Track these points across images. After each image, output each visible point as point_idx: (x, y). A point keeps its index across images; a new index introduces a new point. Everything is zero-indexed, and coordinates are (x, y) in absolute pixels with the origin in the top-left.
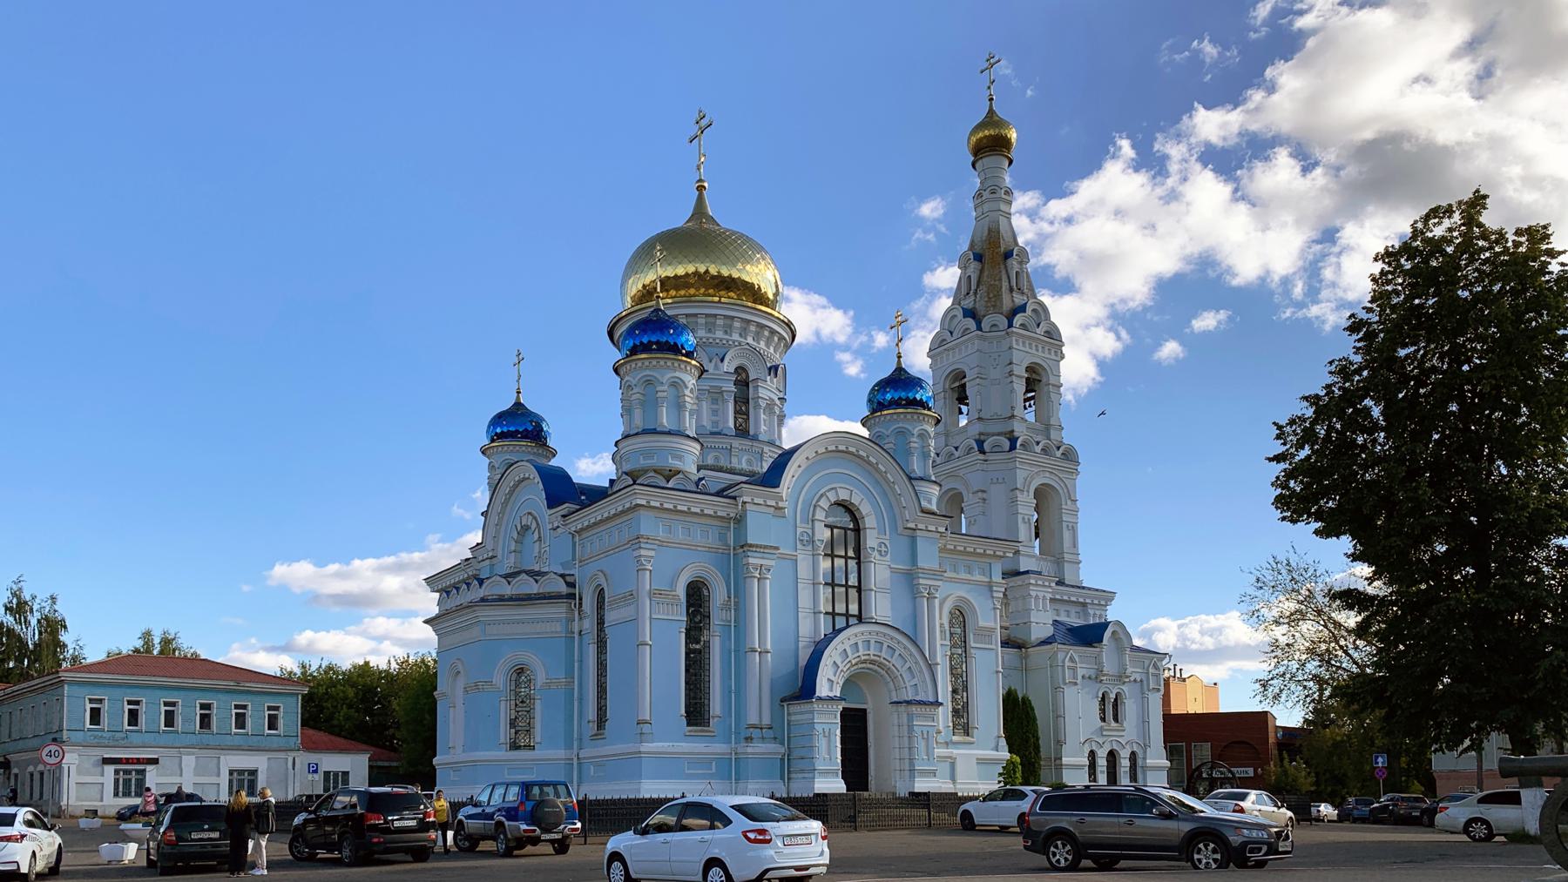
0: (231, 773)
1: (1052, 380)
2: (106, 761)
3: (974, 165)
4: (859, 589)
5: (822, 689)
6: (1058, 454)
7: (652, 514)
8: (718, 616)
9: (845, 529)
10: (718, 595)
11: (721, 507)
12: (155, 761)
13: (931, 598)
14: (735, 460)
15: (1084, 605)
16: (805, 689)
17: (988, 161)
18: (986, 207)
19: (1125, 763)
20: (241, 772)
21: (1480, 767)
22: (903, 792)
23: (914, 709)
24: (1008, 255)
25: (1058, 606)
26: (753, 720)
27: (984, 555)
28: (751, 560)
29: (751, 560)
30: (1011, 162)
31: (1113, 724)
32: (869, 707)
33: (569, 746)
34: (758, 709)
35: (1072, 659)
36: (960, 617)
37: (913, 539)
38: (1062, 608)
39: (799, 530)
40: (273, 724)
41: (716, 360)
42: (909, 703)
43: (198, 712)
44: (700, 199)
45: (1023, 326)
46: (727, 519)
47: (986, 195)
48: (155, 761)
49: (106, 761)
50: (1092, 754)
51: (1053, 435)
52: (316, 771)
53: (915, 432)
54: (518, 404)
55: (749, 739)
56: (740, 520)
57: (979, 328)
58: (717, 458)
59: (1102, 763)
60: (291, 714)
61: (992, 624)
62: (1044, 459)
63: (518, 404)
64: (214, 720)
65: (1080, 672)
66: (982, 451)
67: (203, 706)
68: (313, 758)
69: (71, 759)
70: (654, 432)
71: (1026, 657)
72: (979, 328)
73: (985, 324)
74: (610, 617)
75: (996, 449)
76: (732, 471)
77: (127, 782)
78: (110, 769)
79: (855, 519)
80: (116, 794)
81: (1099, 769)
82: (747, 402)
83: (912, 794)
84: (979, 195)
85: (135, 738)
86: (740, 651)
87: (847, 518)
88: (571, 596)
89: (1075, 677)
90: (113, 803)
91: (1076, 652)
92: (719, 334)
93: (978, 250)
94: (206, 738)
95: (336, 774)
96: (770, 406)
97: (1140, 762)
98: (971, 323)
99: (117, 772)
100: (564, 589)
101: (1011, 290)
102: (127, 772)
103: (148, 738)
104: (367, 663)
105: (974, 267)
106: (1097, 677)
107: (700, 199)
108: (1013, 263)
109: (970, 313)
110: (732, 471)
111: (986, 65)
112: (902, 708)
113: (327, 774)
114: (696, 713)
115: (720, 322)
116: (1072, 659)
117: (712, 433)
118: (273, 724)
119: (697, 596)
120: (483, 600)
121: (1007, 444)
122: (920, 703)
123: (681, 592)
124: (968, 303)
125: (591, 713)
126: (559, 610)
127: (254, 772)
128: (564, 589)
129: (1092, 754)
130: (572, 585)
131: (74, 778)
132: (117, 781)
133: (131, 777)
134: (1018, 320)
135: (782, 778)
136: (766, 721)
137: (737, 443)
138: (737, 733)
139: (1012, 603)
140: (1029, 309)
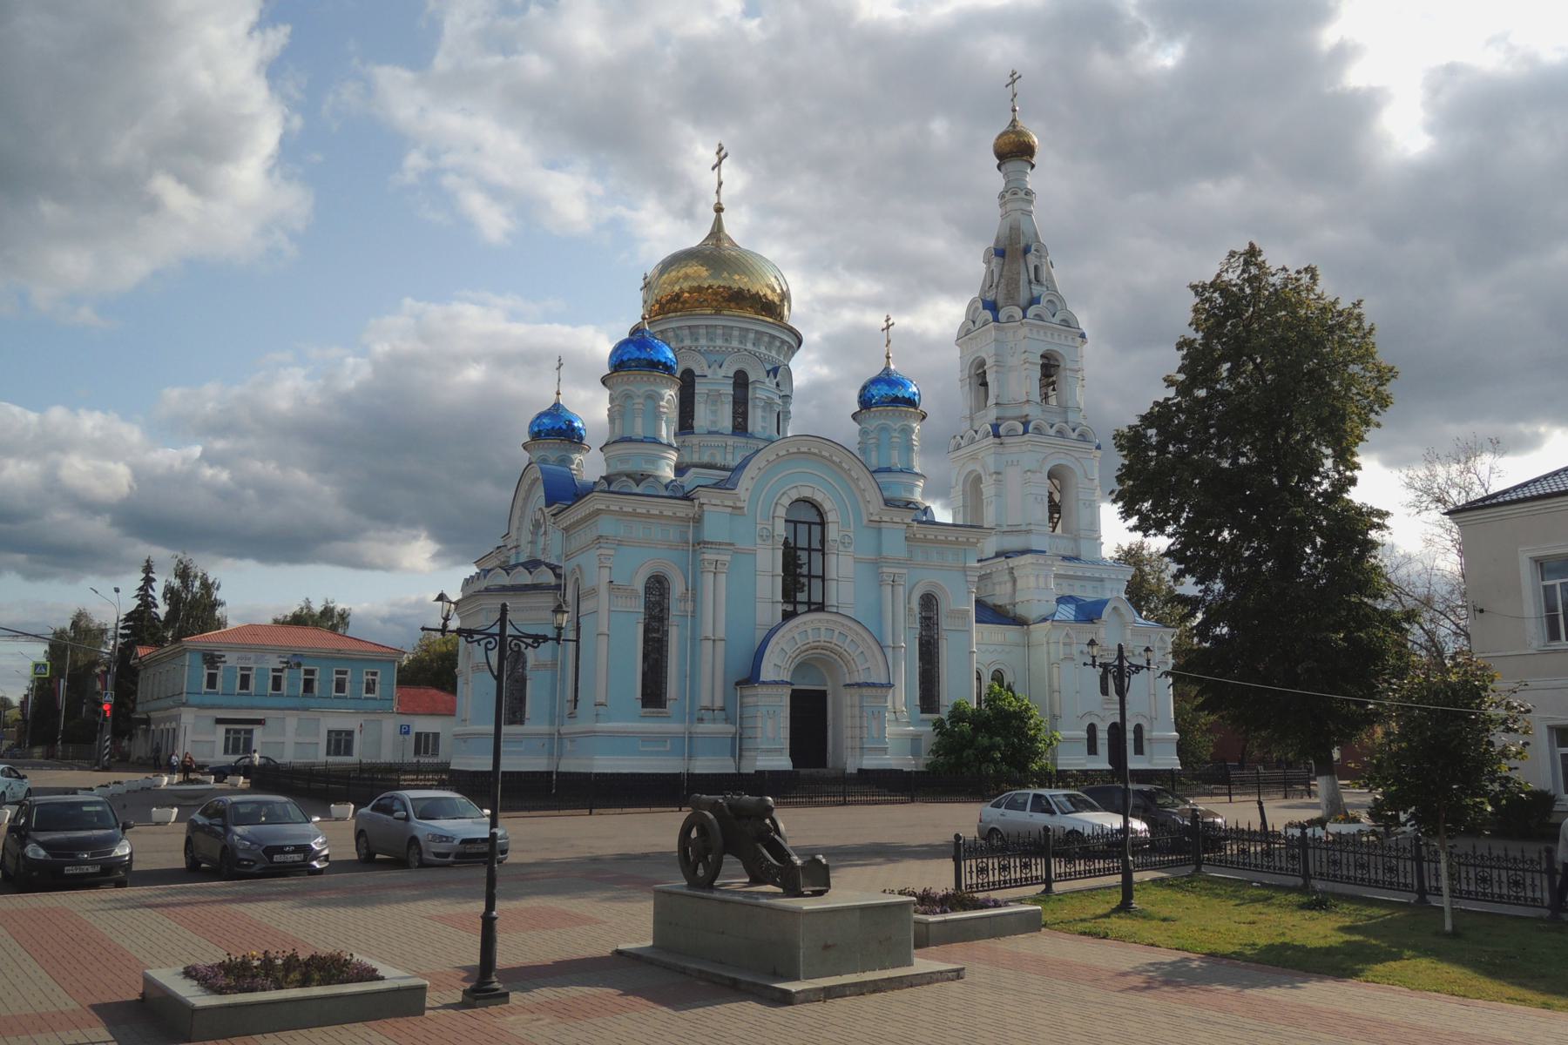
0: (330, 732)
1: (1070, 365)
2: (219, 721)
3: (999, 167)
4: (823, 578)
5: (767, 673)
6: (1074, 435)
8: (675, 608)
9: (810, 524)
10: (677, 588)
11: (682, 509)
12: (260, 722)
14: (729, 457)
15: (1102, 580)
16: (751, 678)
17: (1012, 166)
18: (1009, 207)
19: (1130, 736)
20: (339, 733)
21: (490, 906)
22: (851, 768)
23: (864, 691)
24: (1026, 250)
26: (705, 702)
27: (957, 542)
28: (706, 556)
29: (706, 556)
30: (1033, 166)
32: (829, 688)
33: (552, 723)
34: (711, 689)
40: (370, 688)
41: (716, 366)
42: (859, 685)
43: (302, 676)
44: (718, 222)
45: (1038, 317)
46: (686, 519)
47: (1008, 196)
48: (260, 722)
49: (219, 721)
50: (1092, 729)
51: (1071, 417)
52: (407, 733)
54: (557, 405)
55: (701, 720)
56: (698, 520)
57: (996, 319)
58: (712, 455)
59: (1103, 736)
60: (387, 681)
62: (1059, 441)
63: (557, 405)
64: (316, 684)
66: (997, 435)
67: (307, 672)
68: (405, 720)
69: (188, 717)
70: (630, 440)
71: (1028, 634)
72: (996, 319)
73: (1002, 315)
74: (584, 607)
75: (1011, 433)
76: (724, 468)
77: (237, 740)
78: (222, 729)
79: (821, 514)
80: (226, 752)
81: (1099, 742)
82: (746, 404)
83: (860, 770)
84: (1002, 196)
85: (245, 701)
86: (696, 640)
87: (814, 511)
88: (558, 587)
90: (221, 758)
92: (719, 342)
93: (1001, 246)
94: (310, 702)
95: (427, 735)
96: (769, 404)
97: (1146, 735)
98: (988, 315)
99: (228, 731)
100: (552, 580)
101: (1030, 282)
102: (237, 732)
103: (257, 701)
105: (995, 261)
107: (718, 222)
108: (1032, 259)
109: (992, 306)
110: (724, 468)
112: (855, 690)
113: (418, 735)
114: (653, 694)
115: (736, 333)
117: (710, 433)
118: (370, 688)
119: (657, 587)
120: (487, 590)
121: (1021, 429)
122: (873, 685)
123: (639, 585)
124: (990, 296)
125: (570, 694)
126: (548, 601)
127: (350, 733)
128: (552, 580)
129: (1092, 729)
130: (558, 576)
131: (189, 737)
132: (227, 739)
133: (239, 741)
134: (1032, 311)
135: (733, 755)
136: (719, 703)
137: (731, 441)
138: (691, 714)
140: (1043, 301)
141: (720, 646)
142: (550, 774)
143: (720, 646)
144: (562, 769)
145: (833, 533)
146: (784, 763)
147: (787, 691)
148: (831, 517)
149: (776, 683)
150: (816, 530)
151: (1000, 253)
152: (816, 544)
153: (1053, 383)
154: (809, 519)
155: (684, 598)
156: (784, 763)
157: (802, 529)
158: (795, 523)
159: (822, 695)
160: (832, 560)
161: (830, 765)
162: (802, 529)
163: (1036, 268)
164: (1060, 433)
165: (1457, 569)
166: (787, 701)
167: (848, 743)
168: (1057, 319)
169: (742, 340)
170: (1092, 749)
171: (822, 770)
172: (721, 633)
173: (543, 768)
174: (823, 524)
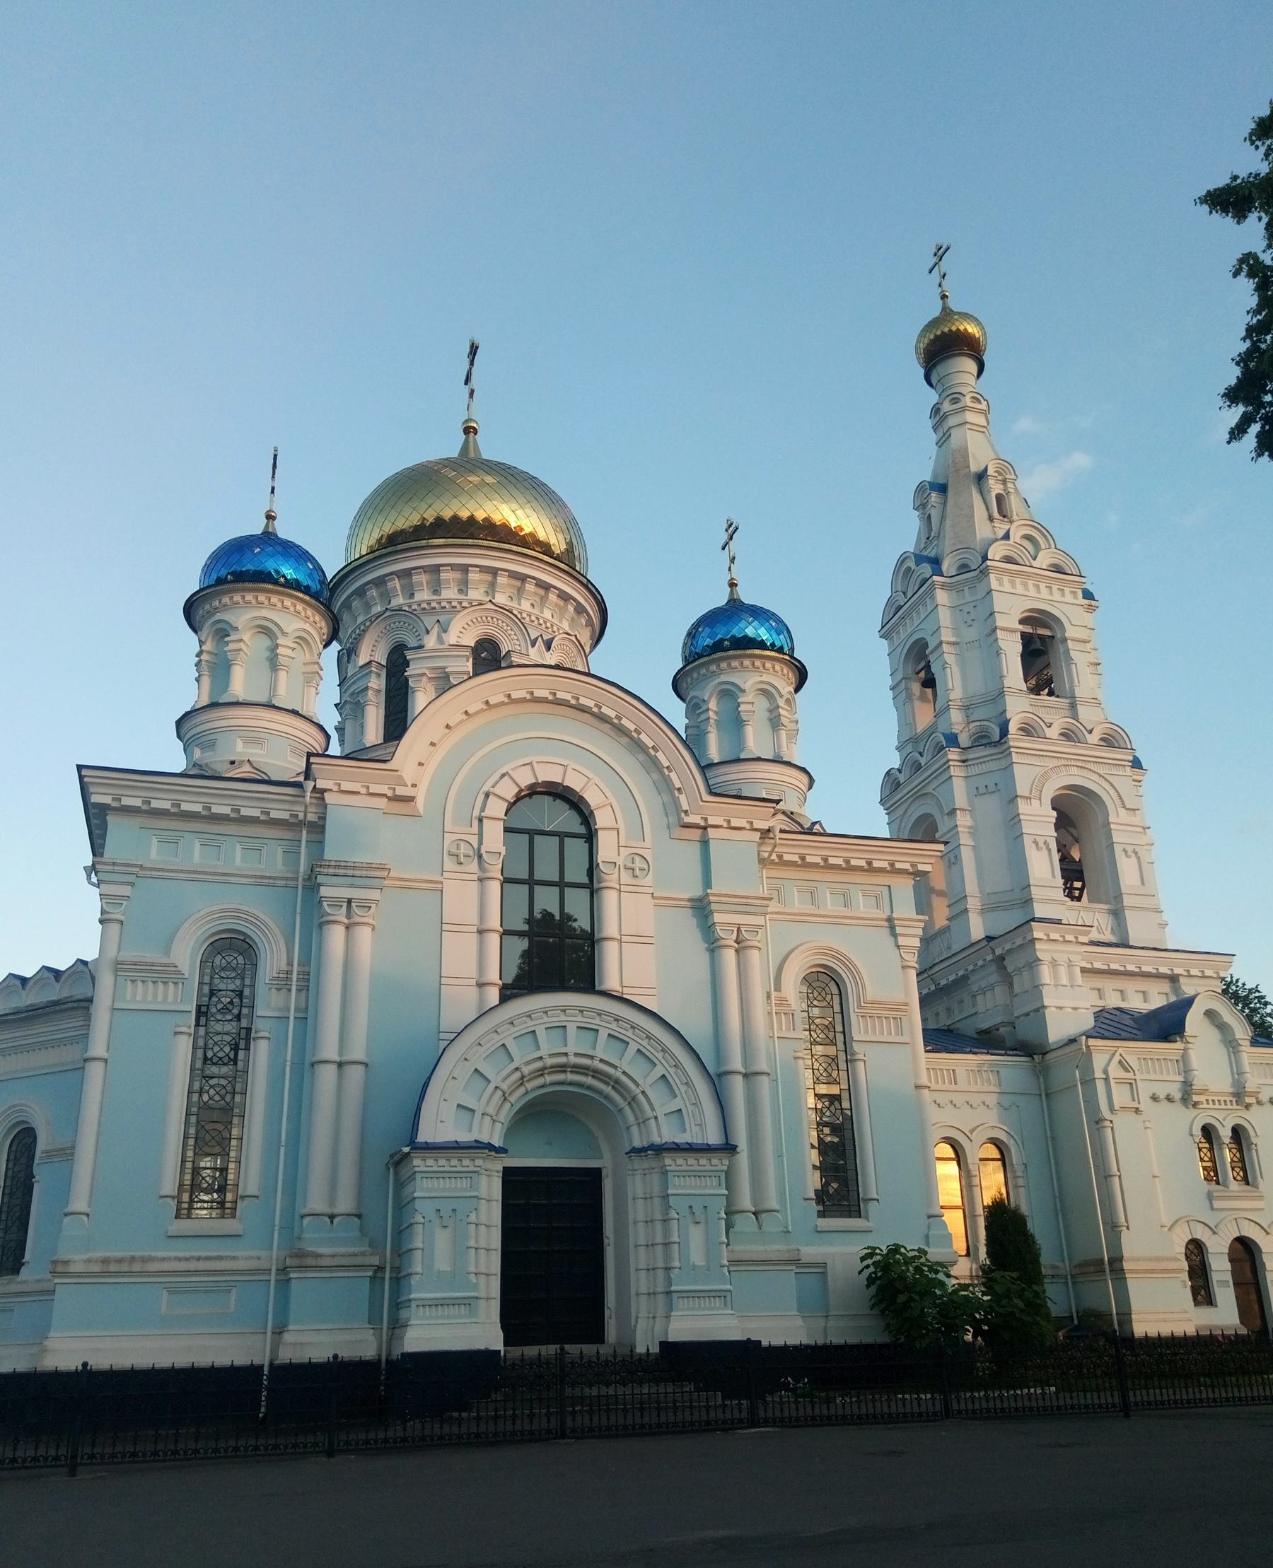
5: (439, 1124)
7: (134, 822)
9: (561, 836)
13: (741, 947)
15: (1174, 979)
22: (645, 1343)
25: (1098, 982)
31: (1234, 1186)
35: (1123, 1065)
36: (827, 983)
37: (705, 843)
38: (1109, 985)
39: (449, 838)
50: (1196, 1250)
53: (747, 686)
59: (1220, 1267)
61: (898, 997)
65: (1145, 1091)
79: (586, 816)
81: (1215, 1278)
83: (665, 1345)
86: (306, 1066)
89: (1134, 1095)
91: (1133, 1051)
101: (991, 519)
104: (336, 1357)
106: (1188, 1096)
111: (935, 260)
116: (1123, 1065)
122: (690, 1149)
123: (186, 954)
129: (1196, 1250)
139: (1016, 980)
141: (356, 1073)
142: (255, 1370)
143: (356, 1073)
144: (287, 1355)
145: (606, 848)
146: (484, 1332)
147: (497, 1166)
148: (602, 819)
149: (456, 1147)
150: (576, 849)
151: (1127, 1416)
152: (576, 873)
153: (1050, 681)
154: (555, 819)
155: (282, 982)
156: (484, 1332)
157: (547, 847)
158: (532, 833)
159: (587, 1184)
160: (609, 900)
161: (611, 1333)
162: (547, 847)
163: (999, 498)
164: (1067, 735)
165: (1143, 1326)
166: (494, 1188)
167: (641, 1283)
168: (1044, 559)
169: (464, 586)
170: (1202, 1292)
171: (589, 1349)
172: (358, 1052)
173: (241, 1360)
174: (590, 837)
